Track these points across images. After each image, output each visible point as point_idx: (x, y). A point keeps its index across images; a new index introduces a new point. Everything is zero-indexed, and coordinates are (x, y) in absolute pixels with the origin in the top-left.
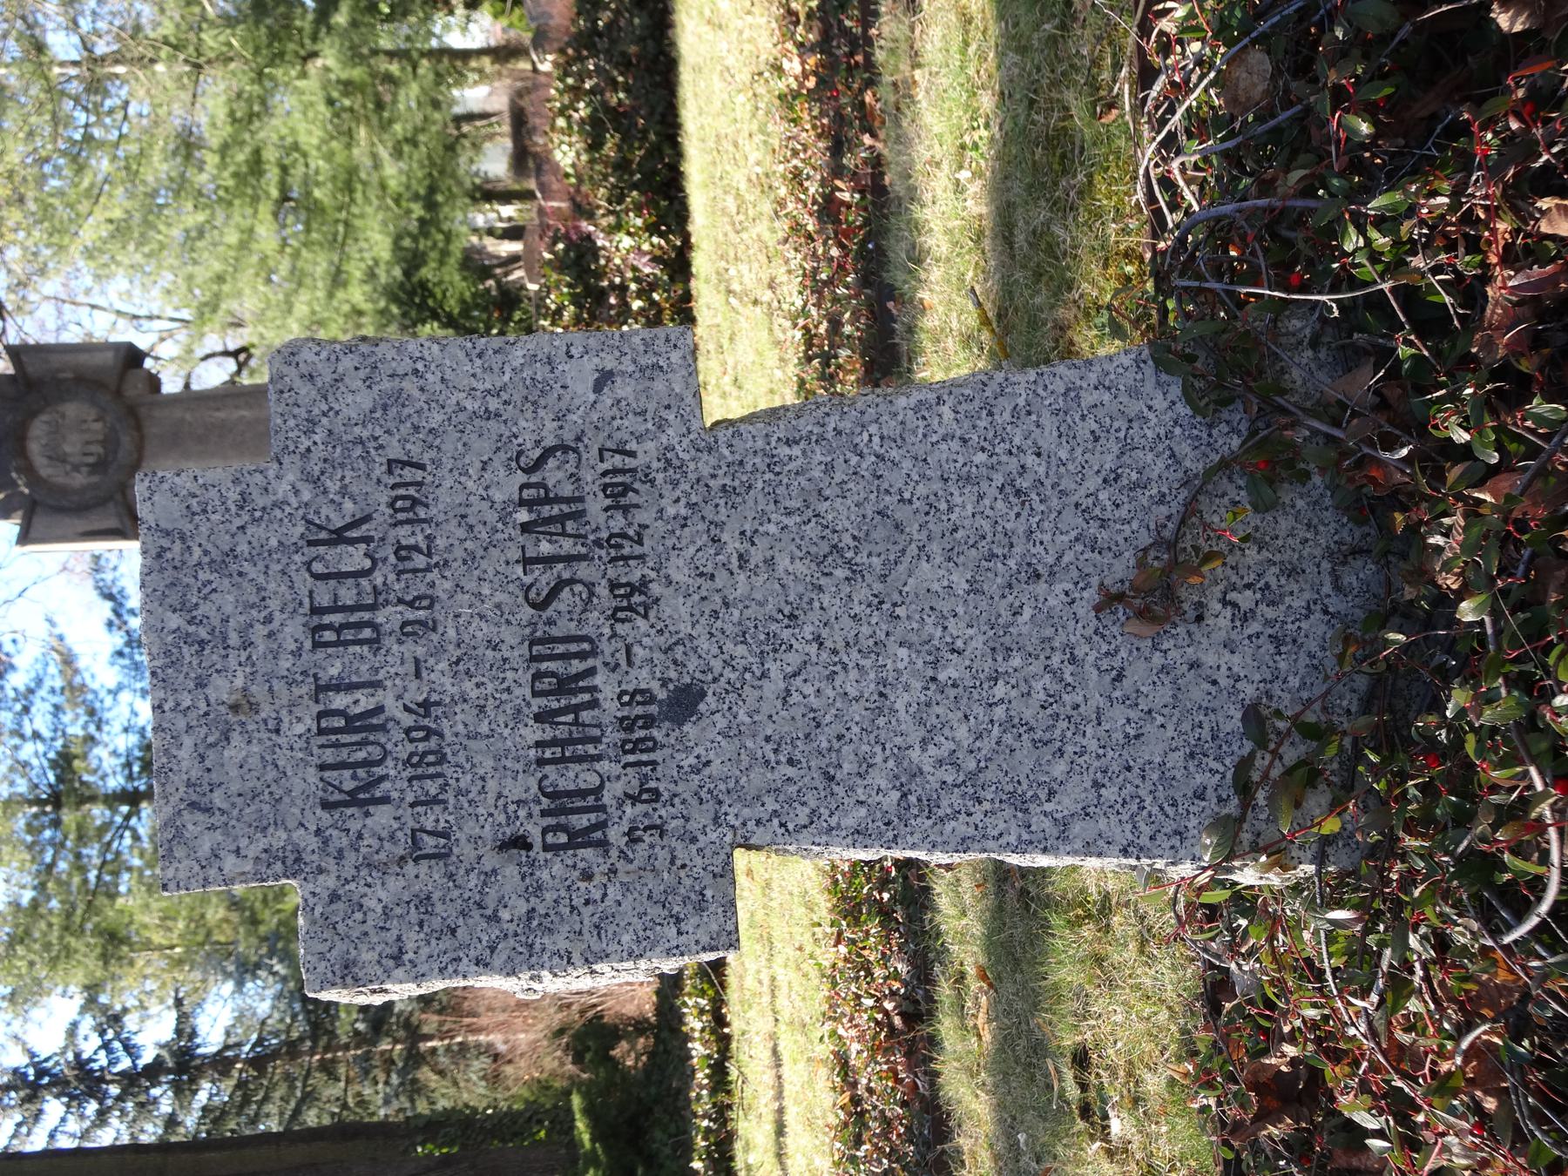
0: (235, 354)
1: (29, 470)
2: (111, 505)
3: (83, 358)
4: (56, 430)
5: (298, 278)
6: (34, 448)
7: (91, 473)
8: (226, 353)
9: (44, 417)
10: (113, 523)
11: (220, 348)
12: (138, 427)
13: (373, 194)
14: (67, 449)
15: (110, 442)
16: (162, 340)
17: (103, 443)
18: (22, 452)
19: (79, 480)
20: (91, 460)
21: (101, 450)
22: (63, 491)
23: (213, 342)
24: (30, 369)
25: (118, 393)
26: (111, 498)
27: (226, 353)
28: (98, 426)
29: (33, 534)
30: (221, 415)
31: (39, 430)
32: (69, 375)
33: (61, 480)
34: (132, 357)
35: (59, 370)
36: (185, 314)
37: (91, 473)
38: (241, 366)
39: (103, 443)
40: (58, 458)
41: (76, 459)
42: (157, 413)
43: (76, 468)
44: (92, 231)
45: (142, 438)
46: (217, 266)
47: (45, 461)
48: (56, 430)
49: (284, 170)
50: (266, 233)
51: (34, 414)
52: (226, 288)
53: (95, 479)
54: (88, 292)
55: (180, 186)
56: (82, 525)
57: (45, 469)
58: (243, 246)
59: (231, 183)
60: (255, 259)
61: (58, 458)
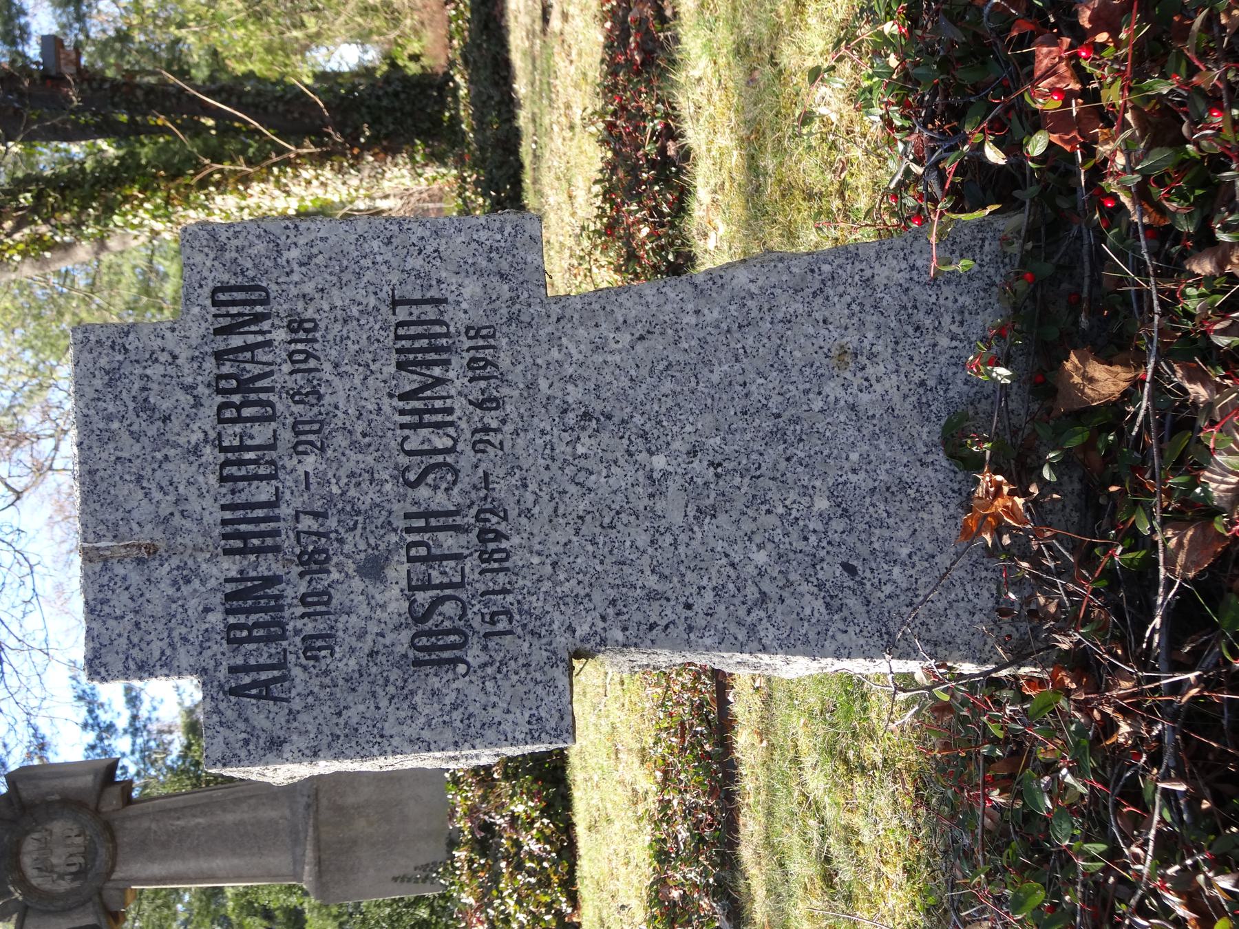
1: (22, 882)
2: (90, 904)
3: (68, 782)
4: (45, 847)
6: (27, 861)
7: (73, 880)
9: (36, 835)
12: (113, 839)
14: (54, 861)
15: (89, 853)
17: (84, 855)
18: (17, 866)
19: (64, 885)
20: (73, 869)
21: (82, 860)
22: (49, 896)
25: (97, 811)
26: (90, 899)
28: (79, 840)
30: (181, 823)
31: (30, 846)
32: (57, 797)
35: (48, 794)
37: (73, 880)
40: (45, 868)
42: (128, 825)
45: (115, 848)
47: (35, 872)
48: (45, 847)
51: (27, 833)
53: (76, 884)
57: (35, 879)
61: (45, 868)
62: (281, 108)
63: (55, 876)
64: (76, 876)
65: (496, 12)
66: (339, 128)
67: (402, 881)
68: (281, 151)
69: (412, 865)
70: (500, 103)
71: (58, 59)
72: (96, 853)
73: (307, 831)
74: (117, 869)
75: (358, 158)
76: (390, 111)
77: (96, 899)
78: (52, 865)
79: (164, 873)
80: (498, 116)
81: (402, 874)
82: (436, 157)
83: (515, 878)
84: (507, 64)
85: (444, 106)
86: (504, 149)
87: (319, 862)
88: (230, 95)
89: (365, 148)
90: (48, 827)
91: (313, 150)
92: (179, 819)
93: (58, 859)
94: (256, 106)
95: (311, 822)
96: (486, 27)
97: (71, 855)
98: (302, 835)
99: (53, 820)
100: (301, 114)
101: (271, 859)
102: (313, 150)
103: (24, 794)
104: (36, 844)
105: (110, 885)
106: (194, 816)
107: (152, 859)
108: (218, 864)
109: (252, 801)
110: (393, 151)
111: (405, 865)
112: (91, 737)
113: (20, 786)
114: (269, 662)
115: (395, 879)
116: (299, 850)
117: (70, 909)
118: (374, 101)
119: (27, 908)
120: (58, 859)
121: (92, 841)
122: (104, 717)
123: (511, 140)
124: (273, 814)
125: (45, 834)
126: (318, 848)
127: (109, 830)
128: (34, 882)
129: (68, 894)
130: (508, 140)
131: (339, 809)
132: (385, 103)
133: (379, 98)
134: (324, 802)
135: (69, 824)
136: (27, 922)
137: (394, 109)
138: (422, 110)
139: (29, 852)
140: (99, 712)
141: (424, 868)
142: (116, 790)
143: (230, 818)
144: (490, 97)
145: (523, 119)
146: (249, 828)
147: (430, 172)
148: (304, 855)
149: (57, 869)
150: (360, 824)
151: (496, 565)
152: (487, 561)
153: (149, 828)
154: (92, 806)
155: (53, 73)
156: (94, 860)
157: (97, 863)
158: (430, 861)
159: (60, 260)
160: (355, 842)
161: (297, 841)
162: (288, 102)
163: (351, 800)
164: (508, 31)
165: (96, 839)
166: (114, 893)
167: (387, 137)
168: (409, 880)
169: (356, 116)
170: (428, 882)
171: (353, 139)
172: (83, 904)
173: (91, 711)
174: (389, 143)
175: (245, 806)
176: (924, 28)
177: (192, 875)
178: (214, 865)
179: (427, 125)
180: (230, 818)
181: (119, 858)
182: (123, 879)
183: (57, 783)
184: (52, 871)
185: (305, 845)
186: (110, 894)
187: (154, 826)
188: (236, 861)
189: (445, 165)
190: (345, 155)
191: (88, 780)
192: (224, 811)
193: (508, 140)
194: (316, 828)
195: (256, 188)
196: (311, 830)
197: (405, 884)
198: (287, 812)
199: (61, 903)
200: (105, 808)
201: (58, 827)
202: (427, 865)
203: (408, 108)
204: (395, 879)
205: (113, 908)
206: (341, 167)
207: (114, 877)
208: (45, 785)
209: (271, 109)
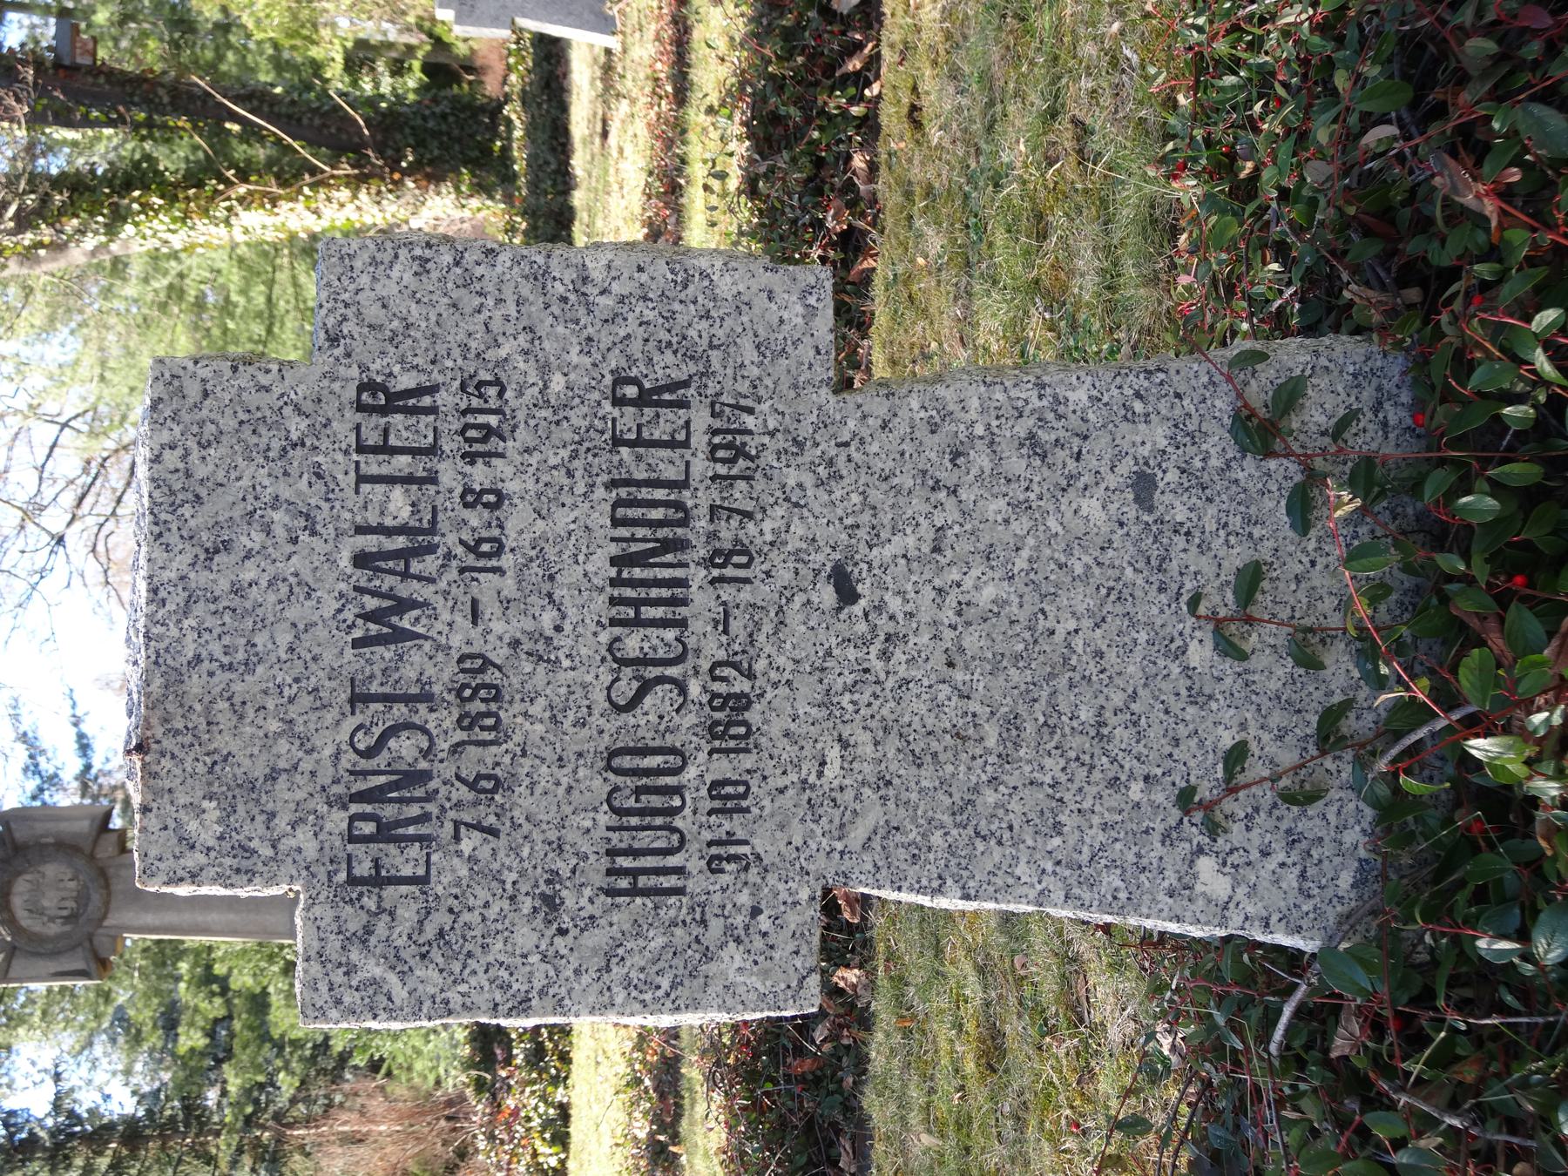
1: (11, 922)
3: (65, 827)
4: (37, 889)
6: (18, 902)
12: (107, 886)
14: (46, 903)
15: (82, 898)
17: (76, 900)
18: (7, 907)
19: (54, 929)
22: (39, 939)
25: (92, 857)
28: (72, 884)
29: (12, 974)
31: (21, 887)
40: (36, 911)
43: (52, 919)
45: (109, 894)
48: (37, 889)
51: (19, 874)
53: (67, 928)
56: (53, 966)
57: (24, 919)
61: (36, 911)
62: (317, 121)
65: (559, 72)
66: (381, 154)
68: (314, 171)
70: (557, 172)
71: (74, 48)
75: (398, 184)
76: (436, 134)
80: (554, 185)
82: (482, 189)
84: (566, 132)
85: (496, 135)
86: (558, 222)
88: (262, 101)
89: (405, 173)
91: (350, 171)
93: (49, 902)
94: (290, 117)
96: (547, 85)
100: (339, 130)
102: (350, 171)
103: (17, 835)
110: (436, 178)
112: (32, 784)
114: (381, 690)
118: (419, 122)
120: (49, 902)
121: (85, 887)
122: (46, 767)
123: (564, 181)
127: (103, 877)
128: (24, 923)
129: (59, 937)
130: (561, 213)
132: (431, 124)
133: (424, 118)
135: (63, 868)
137: (441, 133)
138: (472, 136)
140: (41, 760)
142: (113, 838)
144: (547, 163)
145: (578, 198)
147: (475, 203)
151: (732, 744)
152: (721, 737)
154: (87, 850)
155: (67, 62)
159: (54, 260)
162: (326, 114)
164: (568, 91)
167: (431, 162)
169: (398, 136)
171: (394, 165)
172: (73, 948)
173: (31, 757)
174: (433, 172)
179: (475, 154)
181: (113, 905)
183: (51, 826)
186: (101, 941)
188: (232, 916)
189: (491, 197)
190: (383, 179)
191: (84, 826)
193: (561, 213)
195: (284, 206)
200: (99, 855)
201: (51, 870)
203: (456, 132)
205: (103, 954)
206: (379, 193)
208: (40, 828)
209: (305, 121)
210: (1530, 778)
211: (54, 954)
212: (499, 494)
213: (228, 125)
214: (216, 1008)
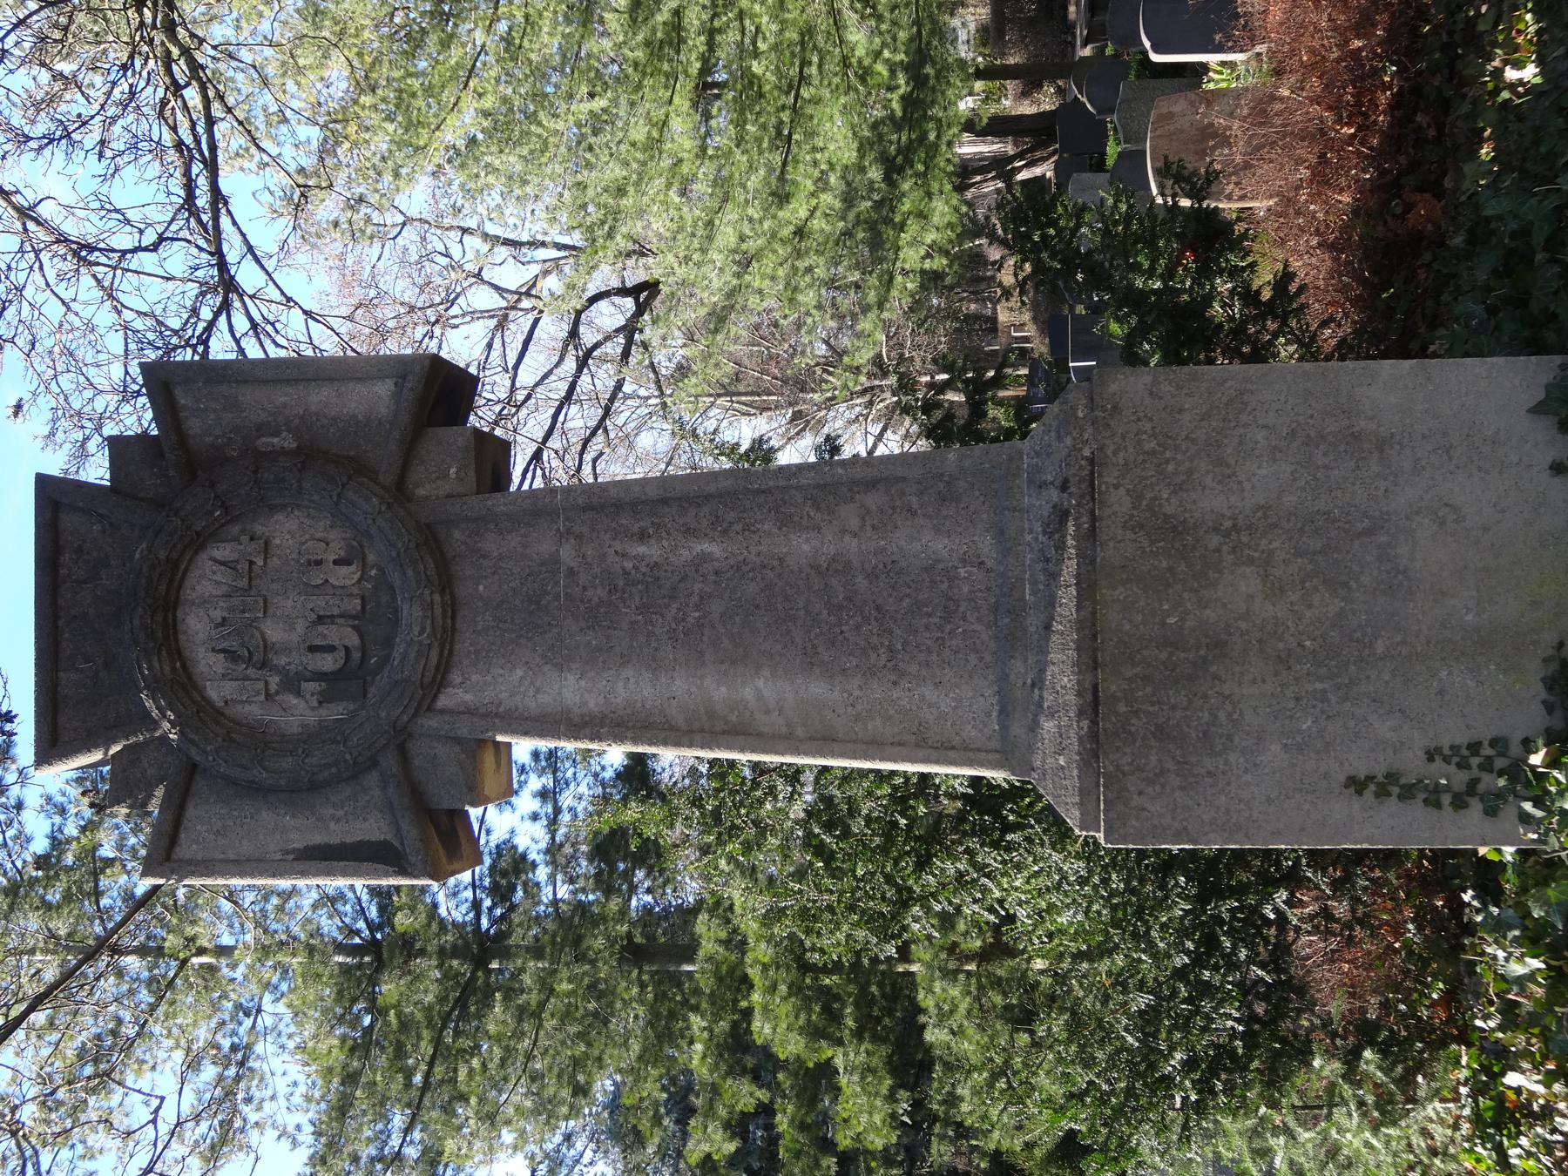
0: (634, 292)
1: (181, 687)
2: (372, 779)
3: (320, 398)
4: (249, 583)
5: (724, 189)
6: (197, 626)
7: (325, 699)
8: (623, 291)
9: (223, 551)
10: (372, 828)
11: (615, 283)
12: (445, 582)
13: (832, 66)
14: (274, 632)
15: (374, 617)
16: (546, 273)
17: (359, 621)
18: (168, 640)
19: (299, 713)
20: (328, 663)
21: (353, 640)
22: (259, 740)
23: (605, 276)
24: (194, 426)
25: (400, 491)
26: (374, 763)
27: (623, 291)
28: (346, 576)
29: (186, 850)
30: (648, 551)
31: (207, 580)
32: (287, 442)
33: (254, 711)
34: (444, 390)
35: (261, 429)
36: (576, 239)
37: (325, 699)
38: (640, 310)
39: (359, 621)
40: (250, 656)
41: (293, 661)
42: (491, 544)
43: (292, 683)
44: (464, 122)
45: (452, 608)
46: (616, 172)
47: (218, 663)
48: (249, 583)
49: (711, 33)
50: (681, 126)
51: (199, 542)
52: (627, 202)
53: (335, 712)
54: (457, 210)
55: (571, 58)
56: (301, 831)
57: (219, 684)
58: (653, 146)
59: (640, 54)
60: (666, 163)
61: (250, 656)
63: (274, 681)
64: (336, 684)
67: (1382, 793)
69: (1421, 740)
72: (395, 622)
73: (1052, 602)
74: (456, 677)
77: (390, 762)
78: (267, 647)
79: (593, 704)
81: (1380, 771)
83: (454, 1114)
87: (1093, 704)
90: (259, 529)
92: (643, 537)
95: (1069, 569)
97: (321, 620)
98: (1033, 622)
99: (273, 509)
101: (929, 692)
104: (222, 575)
105: (432, 722)
106: (690, 532)
107: (558, 658)
108: (760, 690)
109: (873, 500)
111: (1395, 740)
113: (183, 399)
115: (1357, 785)
116: (1019, 669)
117: (314, 787)
119: (192, 769)
124: (940, 546)
125: (251, 548)
126: (1090, 655)
127: (433, 552)
128: (216, 692)
131: (1171, 531)
134: (1118, 502)
136: (191, 812)
139: (204, 602)
141: (1462, 755)
143: (802, 547)
146: (861, 582)
148: (1039, 683)
149: (281, 661)
150: (1240, 588)
153: (555, 560)
156: (388, 643)
157: (397, 652)
158: (1485, 733)
160: (1219, 646)
161: (1014, 631)
163: (1211, 502)
165: (396, 578)
166: (443, 751)
168: (1407, 793)
170: (1476, 806)
172: (354, 773)
175: (850, 515)
176: (1247, 230)
177: (680, 721)
178: (748, 693)
180: (802, 547)
181: (463, 646)
182: (470, 711)
184: (263, 665)
185: (1043, 651)
187: (567, 554)
188: (817, 689)
192: (785, 522)
194: (1087, 589)
196: (1067, 598)
197: (1392, 804)
198: (986, 545)
199: (287, 763)
201: (287, 531)
202: (1474, 747)
204: (1357, 785)
207: (443, 701)
210: (106, 754)
211: (301, 791)
212: (1115, 407)
213: (946, 376)
214: (746, 1095)
